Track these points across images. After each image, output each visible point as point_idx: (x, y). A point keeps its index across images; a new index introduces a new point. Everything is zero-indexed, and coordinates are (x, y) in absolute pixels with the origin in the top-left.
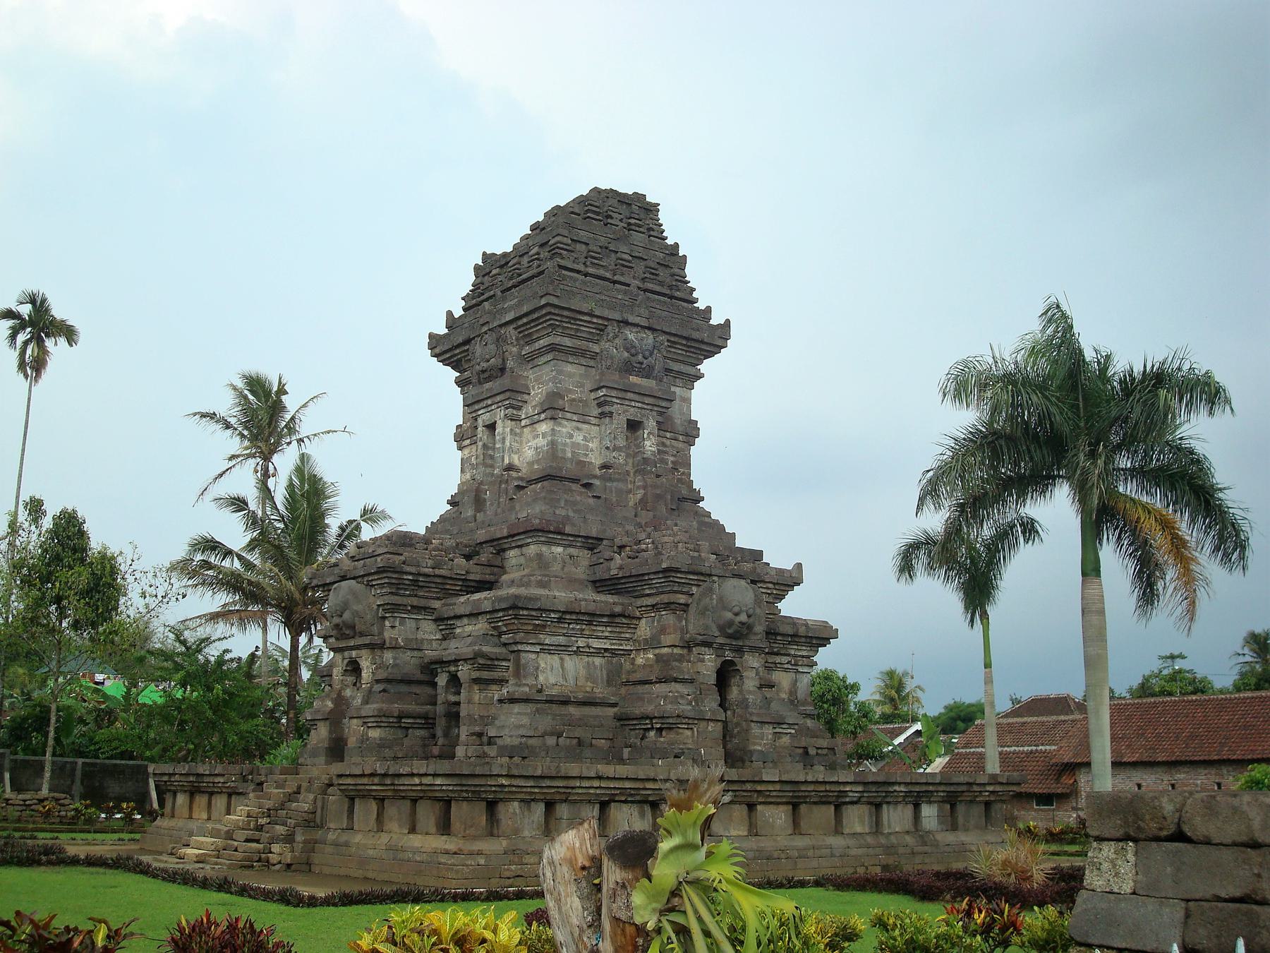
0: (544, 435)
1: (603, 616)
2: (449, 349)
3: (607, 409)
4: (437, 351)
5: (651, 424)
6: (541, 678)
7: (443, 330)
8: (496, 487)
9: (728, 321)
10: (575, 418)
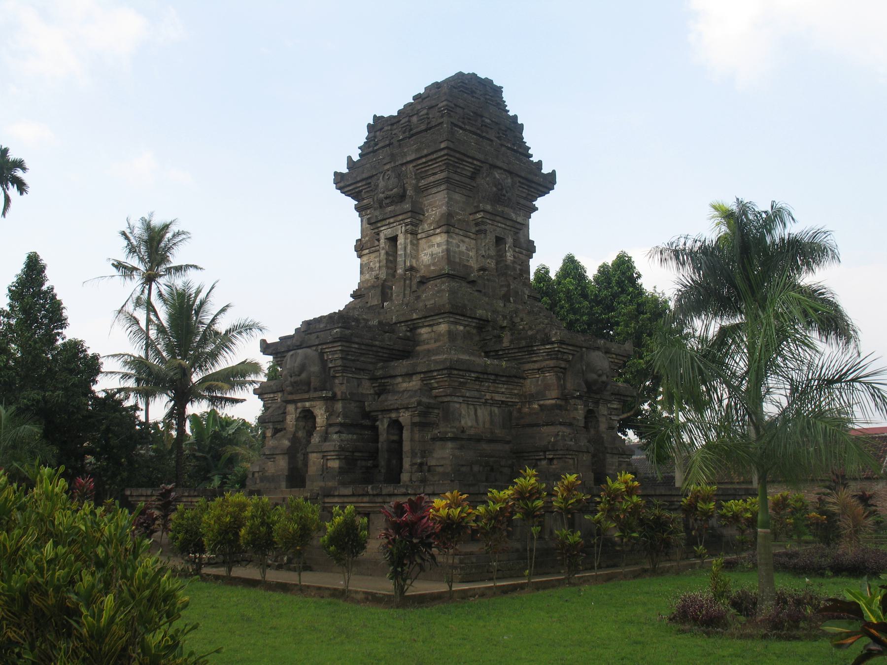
0: (439, 245)
1: (503, 376)
2: (349, 183)
3: (483, 227)
4: (342, 184)
5: (510, 241)
6: (463, 422)
7: (345, 170)
8: (402, 283)
9: (554, 171)
10: (461, 233)
